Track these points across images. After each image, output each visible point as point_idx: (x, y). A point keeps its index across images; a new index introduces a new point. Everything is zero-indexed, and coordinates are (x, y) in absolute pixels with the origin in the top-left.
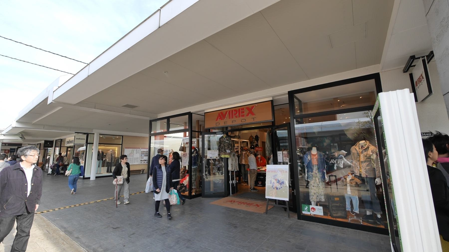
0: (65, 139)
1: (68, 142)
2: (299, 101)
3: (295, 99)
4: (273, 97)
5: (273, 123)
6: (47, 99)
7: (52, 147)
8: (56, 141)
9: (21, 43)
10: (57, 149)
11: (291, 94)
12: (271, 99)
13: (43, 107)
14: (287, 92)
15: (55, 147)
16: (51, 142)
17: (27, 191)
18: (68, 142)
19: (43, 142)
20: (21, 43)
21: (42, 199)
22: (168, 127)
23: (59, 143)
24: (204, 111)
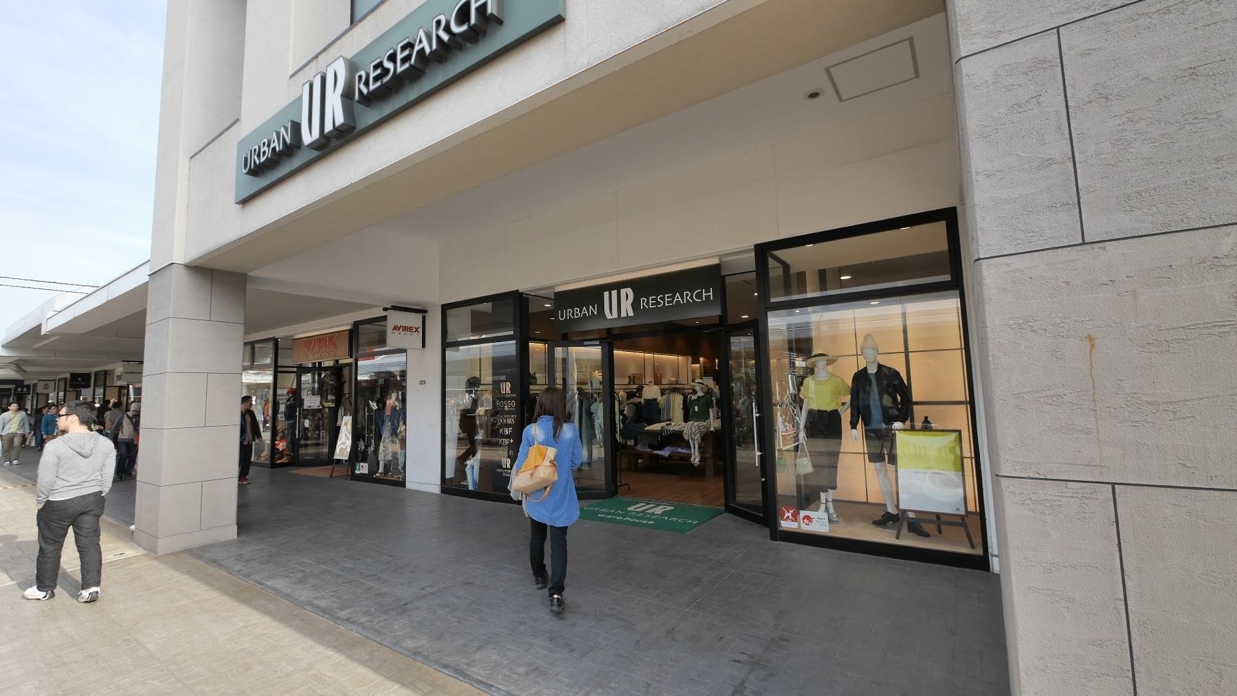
0: (113, 371)
1: (119, 377)
2: (786, 267)
3: (770, 260)
4: (721, 256)
5: (722, 318)
6: (39, 326)
7: (88, 386)
8: (96, 374)
9: (316, 57)
10: (100, 391)
11: (763, 251)
12: (715, 261)
13: (34, 334)
14: (750, 244)
15: (95, 385)
16: (86, 377)
17: (553, 549)
18: (119, 377)
19: (68, 376)
20: (316, 57)
21: (106, 510)
22: (253, 361)
23: (101, 382)
24: (553, 287)
